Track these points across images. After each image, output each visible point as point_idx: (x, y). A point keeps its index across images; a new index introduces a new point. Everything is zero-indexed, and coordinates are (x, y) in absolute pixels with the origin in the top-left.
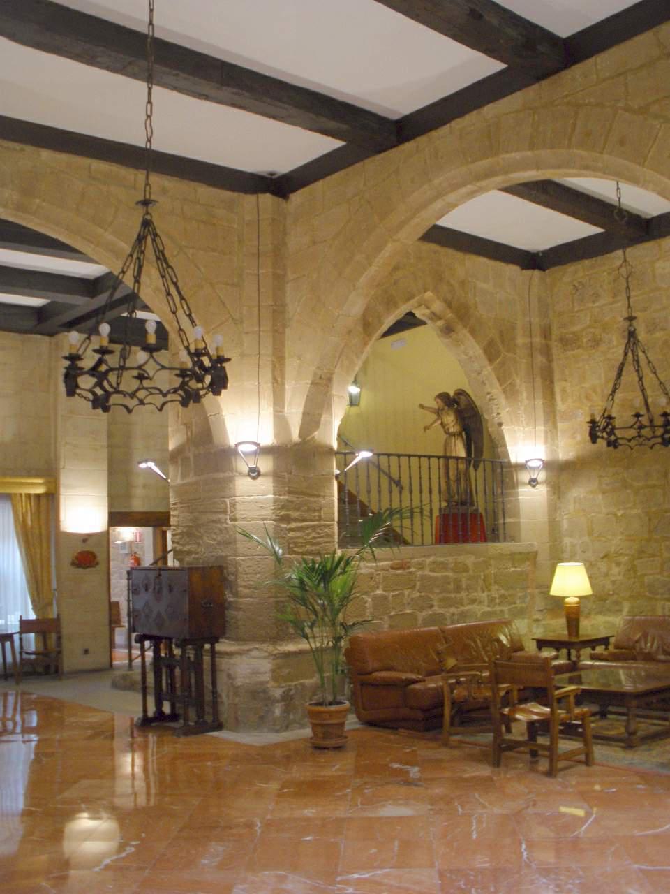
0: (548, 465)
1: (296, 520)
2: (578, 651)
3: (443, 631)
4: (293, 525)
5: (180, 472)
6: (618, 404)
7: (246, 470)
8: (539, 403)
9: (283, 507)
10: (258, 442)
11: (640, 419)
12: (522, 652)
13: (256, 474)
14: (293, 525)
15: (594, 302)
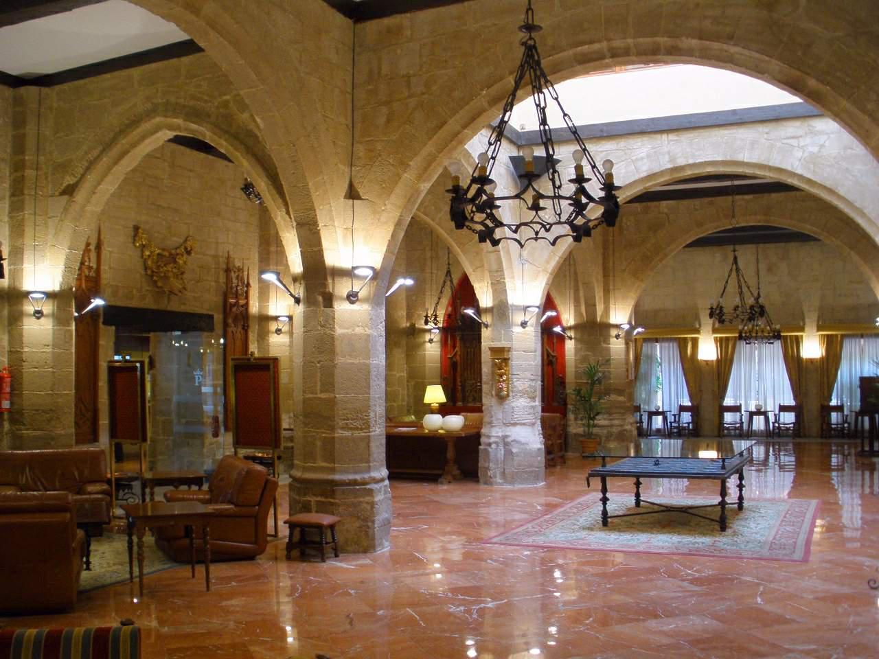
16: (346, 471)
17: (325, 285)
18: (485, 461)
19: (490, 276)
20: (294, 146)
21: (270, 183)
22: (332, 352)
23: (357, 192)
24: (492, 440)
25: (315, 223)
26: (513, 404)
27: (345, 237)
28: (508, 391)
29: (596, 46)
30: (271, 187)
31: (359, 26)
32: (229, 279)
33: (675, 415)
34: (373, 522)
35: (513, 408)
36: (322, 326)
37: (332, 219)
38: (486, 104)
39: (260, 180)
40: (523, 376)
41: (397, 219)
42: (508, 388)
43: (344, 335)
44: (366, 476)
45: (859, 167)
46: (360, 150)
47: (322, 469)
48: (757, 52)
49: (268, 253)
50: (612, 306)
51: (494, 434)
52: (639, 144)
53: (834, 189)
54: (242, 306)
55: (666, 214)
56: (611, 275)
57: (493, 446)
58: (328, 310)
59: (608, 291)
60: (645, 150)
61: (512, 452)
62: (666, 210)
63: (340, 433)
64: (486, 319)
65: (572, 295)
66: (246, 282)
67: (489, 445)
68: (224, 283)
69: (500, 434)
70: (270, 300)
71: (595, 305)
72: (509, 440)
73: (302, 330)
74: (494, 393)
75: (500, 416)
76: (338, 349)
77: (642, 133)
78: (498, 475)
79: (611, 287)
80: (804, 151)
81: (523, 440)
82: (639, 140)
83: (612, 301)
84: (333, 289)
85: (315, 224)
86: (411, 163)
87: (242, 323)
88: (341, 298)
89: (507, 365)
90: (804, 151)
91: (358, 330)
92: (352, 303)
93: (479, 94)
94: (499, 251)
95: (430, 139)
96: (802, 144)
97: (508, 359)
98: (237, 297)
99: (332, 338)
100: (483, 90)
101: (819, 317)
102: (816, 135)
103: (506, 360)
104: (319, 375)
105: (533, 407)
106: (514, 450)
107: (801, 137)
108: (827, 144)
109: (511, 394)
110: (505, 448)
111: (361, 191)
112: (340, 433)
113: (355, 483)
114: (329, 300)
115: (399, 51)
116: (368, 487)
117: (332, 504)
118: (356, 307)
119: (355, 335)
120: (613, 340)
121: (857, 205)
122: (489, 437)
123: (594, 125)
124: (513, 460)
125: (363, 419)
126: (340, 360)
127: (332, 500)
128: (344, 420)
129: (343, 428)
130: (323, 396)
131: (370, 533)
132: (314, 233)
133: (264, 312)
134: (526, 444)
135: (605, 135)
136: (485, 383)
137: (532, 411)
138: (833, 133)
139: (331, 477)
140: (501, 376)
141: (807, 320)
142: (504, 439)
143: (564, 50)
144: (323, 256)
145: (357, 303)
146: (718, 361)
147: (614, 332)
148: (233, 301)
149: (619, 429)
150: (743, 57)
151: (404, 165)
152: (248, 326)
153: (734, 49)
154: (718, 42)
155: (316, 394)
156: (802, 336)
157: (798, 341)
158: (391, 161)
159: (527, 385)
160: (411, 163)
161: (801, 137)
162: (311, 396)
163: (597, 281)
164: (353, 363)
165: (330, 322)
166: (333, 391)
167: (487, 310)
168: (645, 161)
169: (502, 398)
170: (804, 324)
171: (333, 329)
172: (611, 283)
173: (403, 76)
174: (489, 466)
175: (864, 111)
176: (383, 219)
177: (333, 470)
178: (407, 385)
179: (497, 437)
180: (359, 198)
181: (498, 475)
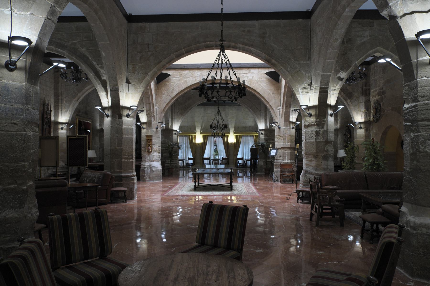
1: (269, 141)
4: (268, 142)
9: (266, 139)
14: (268, 142)
16: (125, 173)
17: (119, 111)
18: (143, 174)
19: (147, 112)
20: (115, 64)
21: (95, 75)
22: (122, 133)
23: (129, 81)
24: (146, 166)
25: (118, 91)
26: (153, 154)
27: (126, 95)
28: (151, 150)
29: (212, 43)
30: (96, 77)
31: (130, 24)
32: (44, 108)
33: (187, 161)
34: (134, 189)
35: (153, 156)
36: (118, 125)
37: (123, 90)
38: (174, 57)
39: (90, 73)
40: (156, 145)
41: (143, 91)
42: (151, 149)
43: (125, 128)
44: (132, 174)
45: (264, 84)
46: (130, 67)
47: (117, 172)
48: (259, 50)
49: (58, 99)
50: (174, 124)
51: (146, 164)
52: (197, 72)
53: (256, 90)
54: (49, 118)
55: (193, 94)
56: (174, 113)
57: (146, 168)
58: (120, 120)
59: (173, 119)
60: (199, 74)
61: (153, 170)
62: (192, 93)
63: (124, 160)
64: (144, 126)
65: (264, 115)
66: (50, 110)
67: (145, 168)
68: (42, 109)
69: (148, 164)
70: (59, 117)
71: (168, 124)
72: (152, 166)
73: (110, 126)
74: (146, 151)
75: (148, 158)
76: (123, 133)
77: (191, 68)
78: (148, 178)
79: (174, 118)
80: (248, 78)
81: (156, 166)
82: (197, 70)
83: (174, 122)
84: (122, 113)
85: (118, 91)
86: (149, 73)
87: (48, 125)
88: (125, 116)
89: (151, 142)
90: (248, 78)
91: (130, 127)
92: (128, 118)
93: (173, 54)
94: (150, 104)
95: (156, 66)
96: (247, 76)
97: (152, 139)
98: (47, 115)
99: (122, 129)
100: (174, 52)
101: (234, 130)
102: (251, 73)
103: (151, 140)
104: (116, 141)
105: (159, 155)
106: (154, 170)
107: (247, 73)
108: (254, 76)
109: (152, 151)
110: (150, 169)
111: (131, 81)
112: (124, 160)
113: (128, 176)
114: (120, 116)
115: (145, 35)
116: (133, 178)
117: (121, 184)
118: (129, 119)
119: (129, 128)
120: (174, 135)
121: (262, 95)
122: (145, 165)
123: (182, 64)
124: (153, 173)
125: (131, 156)
126: (124, 136)
127: (121, 183)
128: (125, 156)
129: (124, 159)
130: (118, 148)
131: (133, 193)
132: (117, 94)
133: (57, 120)
134: (157, 167)
135: (186, 68)
136: (143, 148)
137: (159, 157)
138: (256, 73)
139: (121, 175)
140: (149, 145)
141: (230, 131)
142: (150, 166)
143: (202, 43)
144: (119, 102)
145: (129, 118)
146: (202, 143)
147: (174, 132)
148: (45, 116)
149: (176, 164)
150: (255, 51)
151: (146, 74)
152: (51, 126)
153: (252, 49)
154: (248, 46)
155: (115, 147)
156: (229, 136)
157: (227, 137)
158: (142, 72)
159: (158, 148)
160: (149, 73)
161: (247, 73)
162: (113, 148)
163: (170, 115)
164: (128, 137)
165: (121, 123)
166: (122, 146)
167: (144, 123)
168: (198, 77)
169: (149, 152)
170: (230, 132)
171: (122, 126)
172: (174, 116)
173: (147, 44)
174: (145, 175)
175: (287, 70)
176: (138, 91)
177: (121, 173)
178: (100, 150)
179: (148, 165)
180: (130, 83)
181: (148, 178)
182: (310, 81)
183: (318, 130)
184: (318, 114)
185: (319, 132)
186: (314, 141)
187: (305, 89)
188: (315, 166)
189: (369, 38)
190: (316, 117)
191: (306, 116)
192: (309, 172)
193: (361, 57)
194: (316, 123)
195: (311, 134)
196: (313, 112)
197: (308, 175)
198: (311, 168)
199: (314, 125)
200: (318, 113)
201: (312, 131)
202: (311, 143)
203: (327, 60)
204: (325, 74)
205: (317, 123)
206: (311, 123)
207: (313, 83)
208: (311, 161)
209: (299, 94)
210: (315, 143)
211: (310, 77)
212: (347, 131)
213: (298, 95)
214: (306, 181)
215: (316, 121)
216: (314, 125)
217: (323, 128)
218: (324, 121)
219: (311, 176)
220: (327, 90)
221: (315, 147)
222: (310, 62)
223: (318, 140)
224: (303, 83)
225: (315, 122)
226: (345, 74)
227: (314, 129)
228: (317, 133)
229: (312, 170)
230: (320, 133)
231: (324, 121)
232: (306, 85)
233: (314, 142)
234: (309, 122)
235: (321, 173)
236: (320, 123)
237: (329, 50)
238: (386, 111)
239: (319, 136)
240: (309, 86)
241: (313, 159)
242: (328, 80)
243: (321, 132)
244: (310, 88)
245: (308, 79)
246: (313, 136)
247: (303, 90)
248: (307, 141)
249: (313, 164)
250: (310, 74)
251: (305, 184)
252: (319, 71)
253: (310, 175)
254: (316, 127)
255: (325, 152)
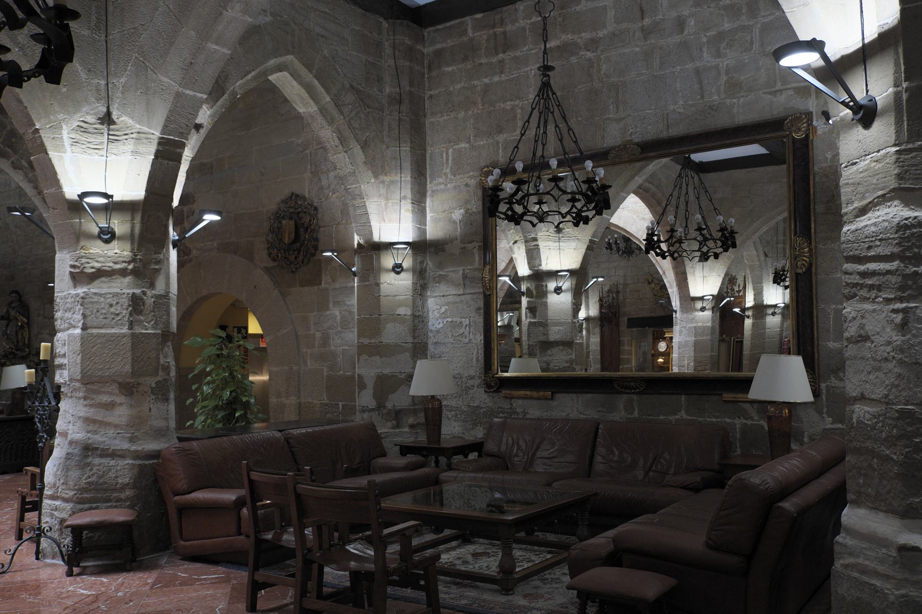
0: (419, 247)
2: (449, 459)
3: (287, 440)
5: (405, 282)
6: (81, 70)
7: (96, 230)
8: (406, 148)
10: (110, 193)
11: (561, 184)
12: (384, 458)
13: (109, 235)
15: (720, 103)
182: (105, 110)
183: (138, 291)
184: (142, 236)
185: (142, 299)
186: (125, 330)
187: (86, 135)
188: (127, 425)
189: (269, 19)
190: (132, 244)
191: (90, 237)
192: (103, 450)
193: (250, 72)
194: (130, 267)
195: (111, 306)
196: (119, 225)
197: (97, 461)
198: (111, 432)
199: (123, 273)
200: (142, 230)
201: (115, 295)
202: (708, 327)
203: (209, 44)
204: (188, 92)
205: (134, 267)
206: (111, 264)
207: (115, 115)
208: (110, 406)
209: (61, 148)
210: (127, 341)
211: (104, 94)
212: (13, 305)
213: (55, 151)
214: (89, 483)
215: (133, 260)
216: (123, 273)
217: (152, 286)
218: (158, 262)
219: (112, 463)
220: (179, 150)
221: (130, 353)
222: (103, 38)
223: (138, 330)
224: (77, 110)
225: (129, 262)
226: (208, 112)
227: (124, 287)
228: (136, 303)
229: (117, 442)
230: (144, 304)
231: (158, 262)
232: (90, 119)
233: (124, 336)
234: (101, 259)
235: (152, 446)
236: (144, 268)
237: (232, 9)
238: (194, 252)
239: (140, 313)
240: (102, 124)
241: (120, 399)
242: (190, 116)
243: (149, 301)
244: (109, 135)
245: (98, 100)
246: (117, 315)
247: (78, 137)
248: (94, 331)
249: (120, 416)
250: (103, 82)
251: (85, 495)
252: (168, 77)
253: (105, 461)
254: (128, 279)
255: (160, 373)
